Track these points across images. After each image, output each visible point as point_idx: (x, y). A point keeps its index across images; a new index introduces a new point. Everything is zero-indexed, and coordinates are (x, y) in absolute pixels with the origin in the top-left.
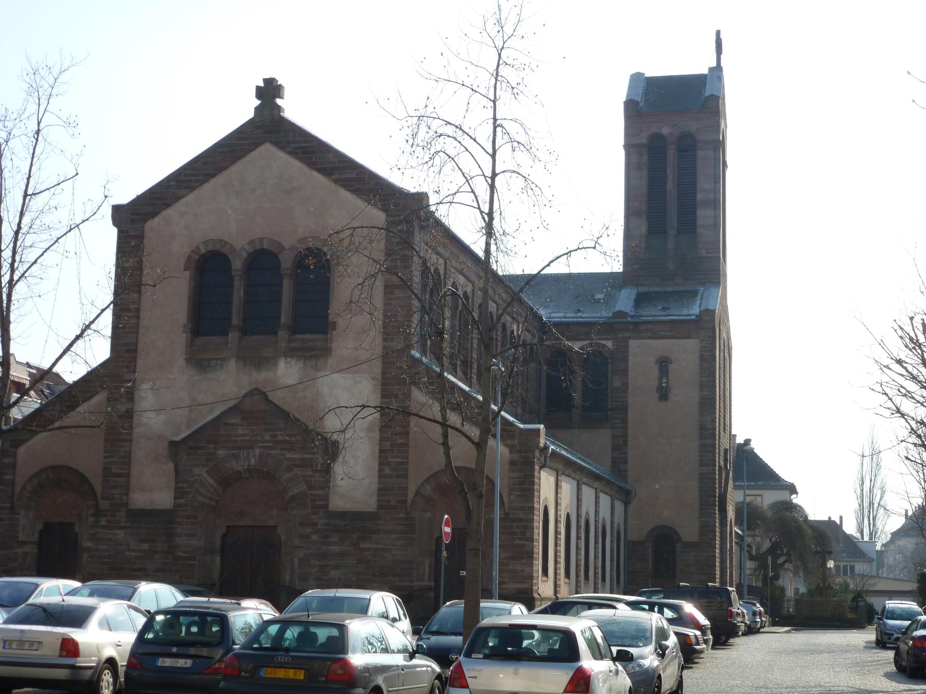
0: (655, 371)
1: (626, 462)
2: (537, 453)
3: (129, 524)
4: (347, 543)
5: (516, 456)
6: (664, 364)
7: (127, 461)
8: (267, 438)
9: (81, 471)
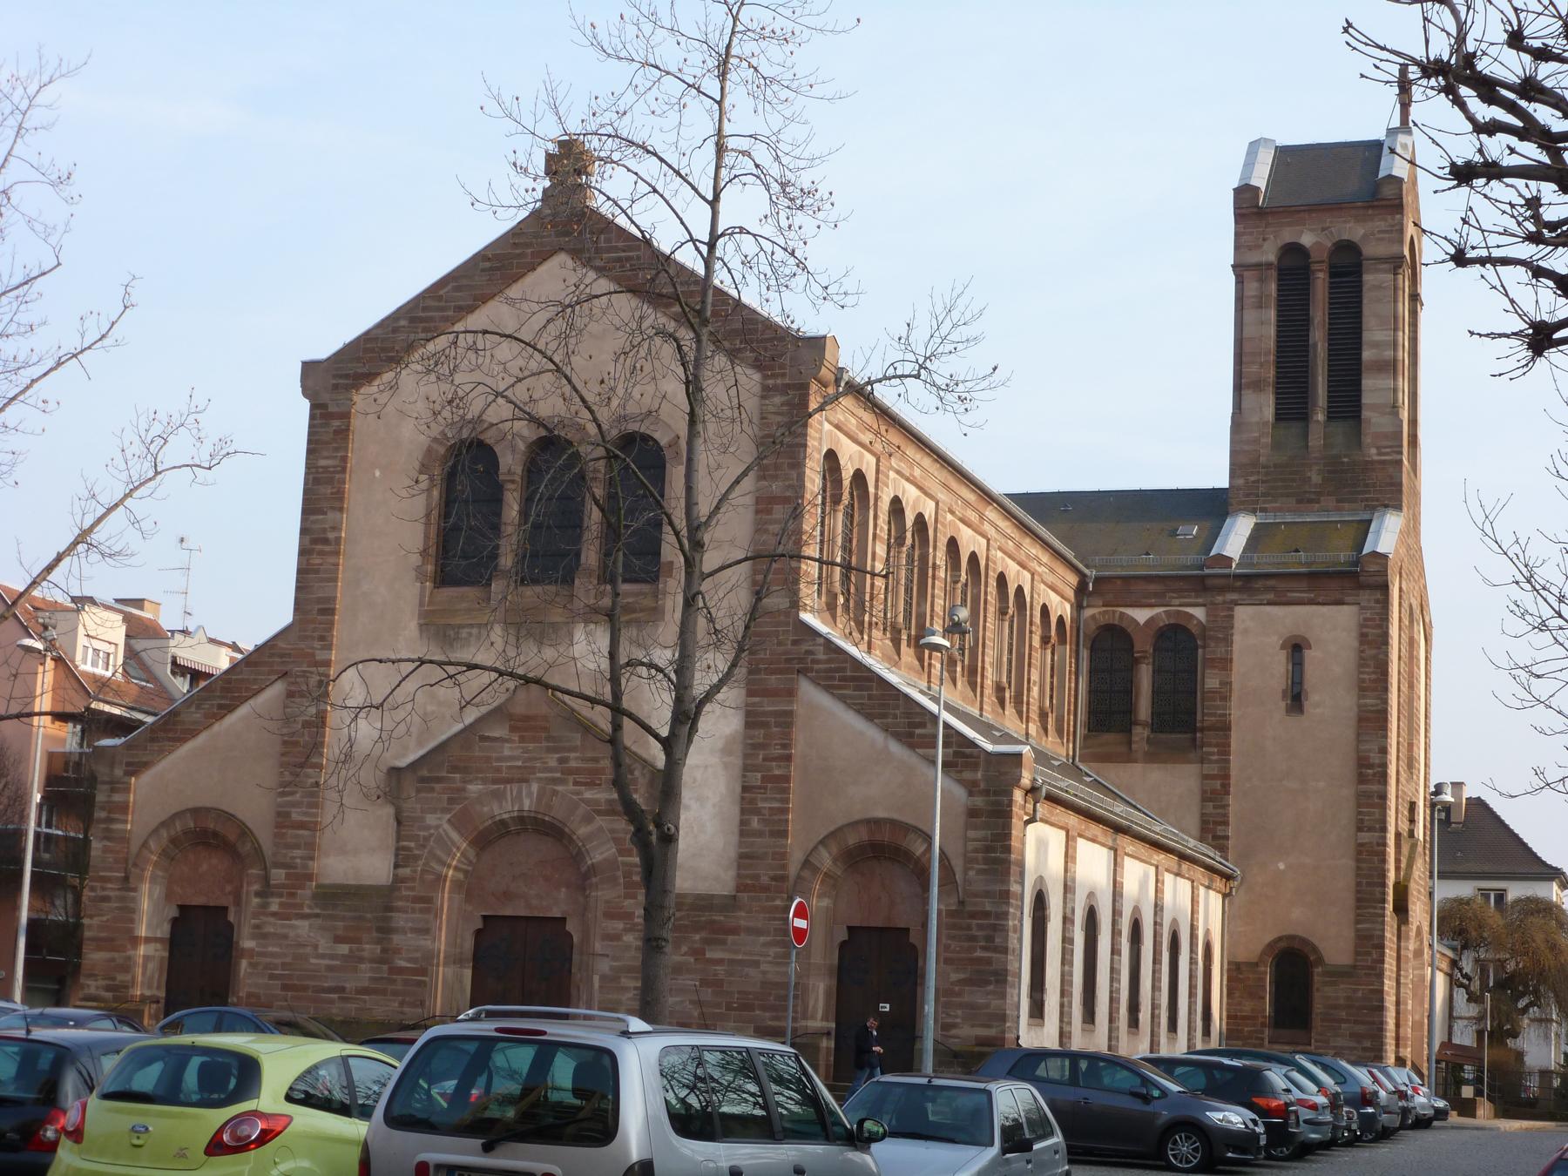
0: (1279, 663)
1: (1226, 823)
2: (1018, 795)
3: (317, 911)
4: (684, 949)
5: (979, 801)
6: (1296, 649)
7: (314, 795)
8: (553, 763)
9: (240, 816)
